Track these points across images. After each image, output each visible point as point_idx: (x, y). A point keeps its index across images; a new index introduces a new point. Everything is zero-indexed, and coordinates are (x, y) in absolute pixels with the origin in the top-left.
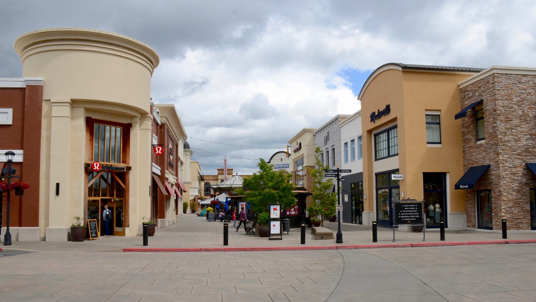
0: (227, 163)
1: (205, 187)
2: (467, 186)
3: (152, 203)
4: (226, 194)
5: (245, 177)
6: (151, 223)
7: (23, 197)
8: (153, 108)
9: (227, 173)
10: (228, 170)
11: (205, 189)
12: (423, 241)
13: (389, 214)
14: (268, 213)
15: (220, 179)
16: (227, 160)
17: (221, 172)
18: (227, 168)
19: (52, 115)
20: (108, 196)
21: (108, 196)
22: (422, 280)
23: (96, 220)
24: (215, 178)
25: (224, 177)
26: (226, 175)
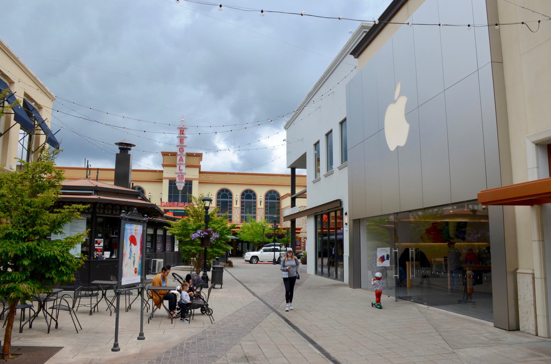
0: (186, 137)
1: (266, 203)
2: (47, 277)
4: (87, 229)
6: (193, 265)
8: (454, 206)
9: (184, 162)
10: (189, 155)
11: (266, 206)
15: (166, 178)
16: (185, 128)
17: (169, 160)
18: (187, 150)
19: (53, 134)
20: (114, 235)
21: (114, 235)
23: (152, 259)
24: (155, 176)
25: (178, 171)
26: (183, 167)
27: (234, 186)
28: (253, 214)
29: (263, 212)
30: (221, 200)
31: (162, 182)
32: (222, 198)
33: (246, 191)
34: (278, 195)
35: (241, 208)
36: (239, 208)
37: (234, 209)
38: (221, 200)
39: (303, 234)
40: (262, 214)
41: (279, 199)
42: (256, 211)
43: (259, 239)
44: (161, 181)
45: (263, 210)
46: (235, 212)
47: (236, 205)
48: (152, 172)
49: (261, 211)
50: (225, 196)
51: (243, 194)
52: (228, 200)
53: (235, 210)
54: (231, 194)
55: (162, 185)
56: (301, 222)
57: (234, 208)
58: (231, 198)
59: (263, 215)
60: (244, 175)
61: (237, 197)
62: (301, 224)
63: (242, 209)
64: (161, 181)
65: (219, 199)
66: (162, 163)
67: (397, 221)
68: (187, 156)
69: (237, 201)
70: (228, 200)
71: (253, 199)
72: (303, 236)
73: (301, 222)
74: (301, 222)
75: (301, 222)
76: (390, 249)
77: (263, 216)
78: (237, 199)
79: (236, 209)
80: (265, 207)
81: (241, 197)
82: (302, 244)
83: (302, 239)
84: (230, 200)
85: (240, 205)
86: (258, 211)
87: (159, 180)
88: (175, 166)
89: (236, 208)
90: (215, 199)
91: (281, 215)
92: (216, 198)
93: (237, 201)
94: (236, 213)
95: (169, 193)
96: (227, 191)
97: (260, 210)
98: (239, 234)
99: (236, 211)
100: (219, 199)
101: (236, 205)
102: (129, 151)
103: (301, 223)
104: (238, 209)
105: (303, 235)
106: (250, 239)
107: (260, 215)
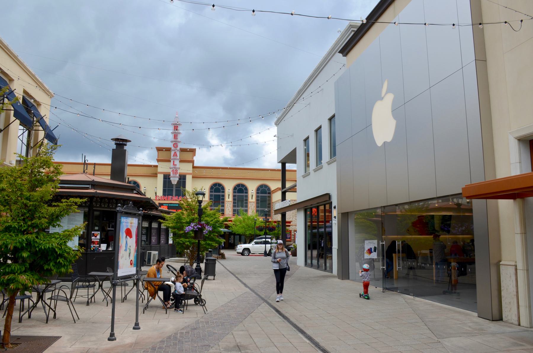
0: (179, 133)
1: (257, 197)
3: (230, 250)
4: (84, 223)
5: (164, 174)
7: (263, 256)
8: (439, 200)
9: (178, 157)
10: (183, 150)
11: (257, 200)
12: (109, 340)
13: (212, 250)
14: (331, 228)
15: (161, 173)
16: (179, 124)
18: (181, 146)
20: (111, 227)
21: (111, 227)
22: (270, 341)
25: (172, 166)
26: (177, 162)
27: (227, 181)
28: (245, 207)
29: (254, 205)
30: (213, 194)
31: (157, 176)
32: (215, 192)
33: (238, 185)
34: (269, 189)
35: (233, 202)
36: (231, 202)
37: (226, 202)
38: (213, 194)
39: (293, 227)
40: (254, 207)
41: (270, 193)
42: (248, 205)
43: (251, 232)
44: (156, 175)
45: (254, 204)
46: (228, 206)
47: (229, 198)
48: (147, 167)
49: (253, 205)
50: (217, 190)
51: (235, 189)
52: (221, 194)
53: (227, 204)
54: (223, 188)
55: (157, 179)
56: (291, 215)
57: (227, 201)
58: (224, 192)
59: (254, 209)
60: (236, 169)
61: (229, 191)
62: (291, 218)
63: (234, 203)
64: (156, 175)
65: (212, 193)
66: (157, 158)
67: (384, 214)
68: (181, 151)
69: (229, 195)
70: (221, 194)
71: (245, 193)
72: (293, 229)
73: (291, 215)
74: (291, 215)
75: (291, 215)
76: (378, 241)
77: (255, 209)
78: (229, 193)
79: (228, 202)
80: (257, 201)
81: (233, 191)
82: (292, 236)
83: (292, 232)
84: (223, 194)
85: (233, 199)
86: (249, 205)
87: (154, 174)
88: (169, 161)
89: (229, 202)
90: (208, 193)
91: (272, 209)
92: (209, 192)
93: (229, 195)
94: (228, 207)
95: (164, 187)
96: (220, 185)
97: (252, 204)
98: (232, 227)
99: (229, 204)
100: (212, 193)
101: (229, 198)
102: (125, 146)
103: (291, 216)
104: (231, 202)
105: (293, 228)
106: (242, 232)
107: (251, 208)
